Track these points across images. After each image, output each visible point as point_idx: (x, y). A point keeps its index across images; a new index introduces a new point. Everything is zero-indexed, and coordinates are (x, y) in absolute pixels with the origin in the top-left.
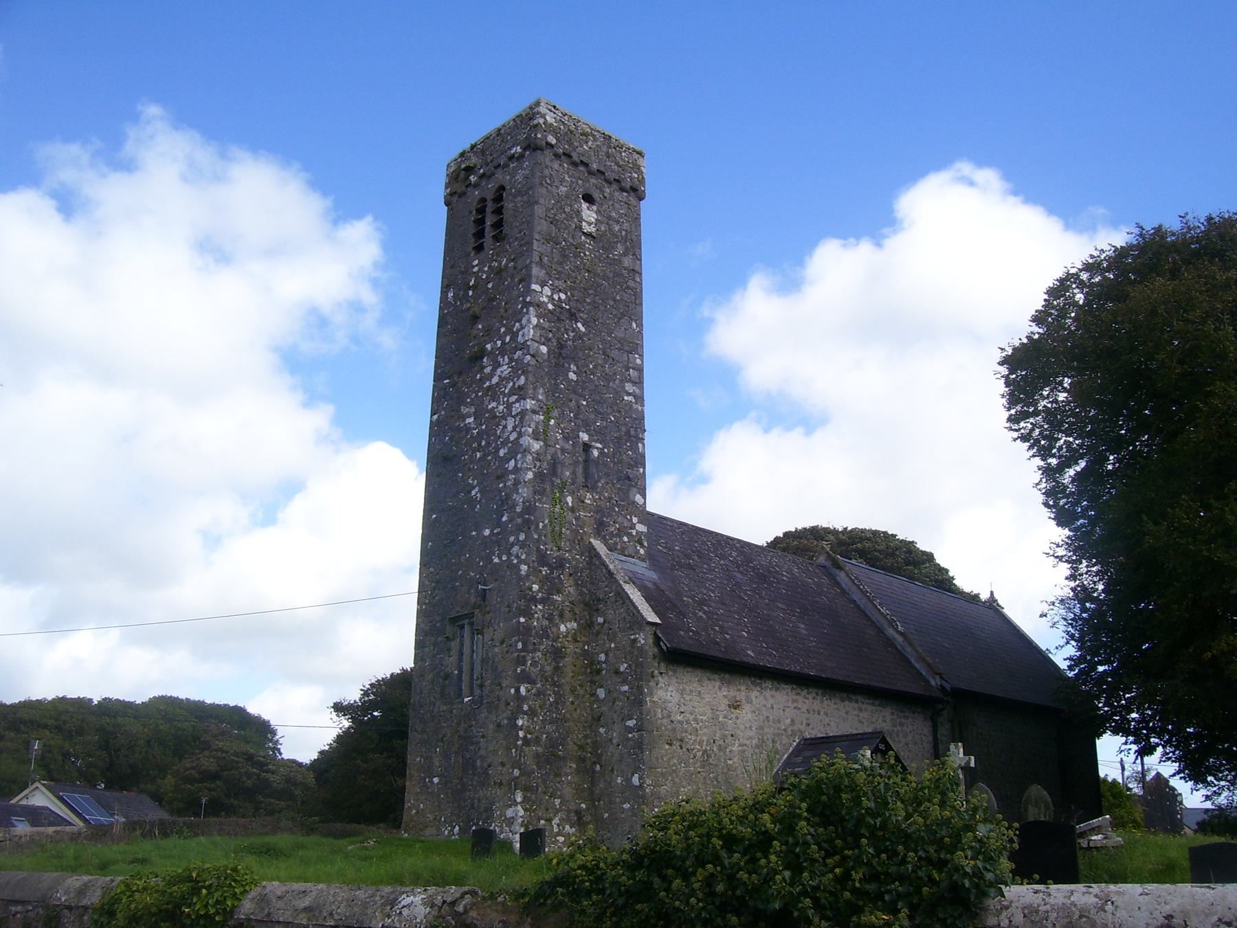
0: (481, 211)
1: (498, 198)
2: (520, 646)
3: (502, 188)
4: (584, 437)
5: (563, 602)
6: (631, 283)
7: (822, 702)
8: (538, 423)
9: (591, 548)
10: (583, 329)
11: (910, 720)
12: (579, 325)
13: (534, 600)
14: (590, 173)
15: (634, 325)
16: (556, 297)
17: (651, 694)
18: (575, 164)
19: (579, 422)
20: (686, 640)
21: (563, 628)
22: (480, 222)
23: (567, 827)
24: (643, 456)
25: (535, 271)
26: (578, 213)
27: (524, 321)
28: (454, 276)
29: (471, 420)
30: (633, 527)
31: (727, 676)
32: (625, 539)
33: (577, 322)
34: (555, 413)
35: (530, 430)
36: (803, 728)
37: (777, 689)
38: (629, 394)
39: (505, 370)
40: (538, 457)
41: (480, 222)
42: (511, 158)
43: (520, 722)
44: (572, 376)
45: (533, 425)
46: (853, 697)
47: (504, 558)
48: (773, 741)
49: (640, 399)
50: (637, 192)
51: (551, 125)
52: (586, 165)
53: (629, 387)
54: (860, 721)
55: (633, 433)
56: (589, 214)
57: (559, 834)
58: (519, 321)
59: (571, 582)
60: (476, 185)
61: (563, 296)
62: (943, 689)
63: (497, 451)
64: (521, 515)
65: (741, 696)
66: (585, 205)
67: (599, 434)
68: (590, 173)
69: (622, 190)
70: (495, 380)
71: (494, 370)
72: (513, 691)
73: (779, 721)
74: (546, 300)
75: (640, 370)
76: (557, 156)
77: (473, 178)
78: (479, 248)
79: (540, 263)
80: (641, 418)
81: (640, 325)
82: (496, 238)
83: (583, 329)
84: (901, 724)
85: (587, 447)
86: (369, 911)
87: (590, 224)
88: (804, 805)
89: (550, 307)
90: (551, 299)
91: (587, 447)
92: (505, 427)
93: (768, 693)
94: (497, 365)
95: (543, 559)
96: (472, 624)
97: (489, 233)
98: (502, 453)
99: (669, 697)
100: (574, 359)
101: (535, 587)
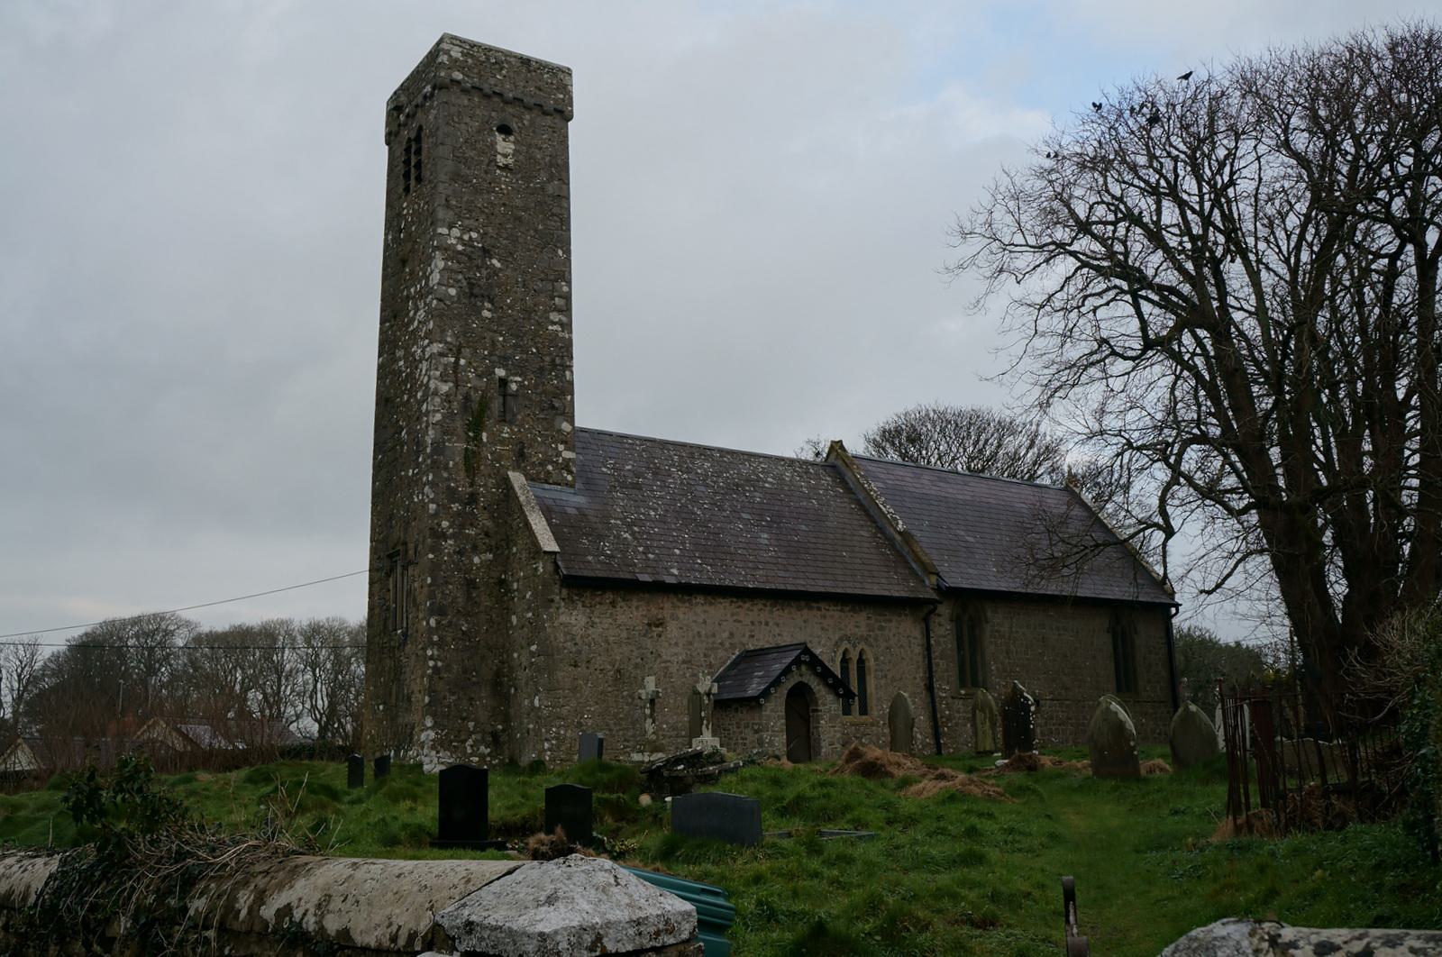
1: (418, 139)
2: (429, 580)
4: (500, 372)
5: (477, 534)
6: (556, 210)
7: (771, 612)
8: (446, 365)
9: (507, 481)
10: (498, 265)
11: (894, 624)
12: (495, 261)
13: (444, 536)
14: (506, 102)
15: (560, 252)
16: (466, 237)
17: (551, 618)
18: (487, 96)
19: (495, 358)
20: (592, 566)
21: (476, 560)
23: (482, 748)
24: (571, 383)
25: (441, 213)
26: (493, 144)
27: (433, 266)
29: (401, 363)
30: (559, 454)
31: (647, 595)
32: (550, 468)
33: (491, 258)
34: (466, 351)
35: (438, 373)
36: (745, 640)
37: (711, 604)
38: (555, 323)
39: (421, 314)
40: (447, 398)
43: (429, 653)
44: (486, 314)
45: (441, 368)
46: (814, 605)
48: (705, 655)
49: (567, 326)
51: (457, 60)
52: (500, 95)
53: (554, 316)
54: (822, 629)
55: (558, 361)
57: (472, 755)
58: (430, 265)
59: (486, 515)
60: (405, 125)
61: (474, 235)
64: (431, 455)
66: (499, 137)
67: (520, 369)
68: (506, 102)
69: (546, 113)
70: (416, 323)
71: (415, 314)
72: (425, 623)
73: (714, 635)
74: (454, 241)
76: (465, 91)
79: (448, 206)
80: (568, 345)
81: (568, 252)
83: (498, 265)
84: (881, 628)
85: (503, 382)
87: (505, 156)
89: (460, 248)
90: (460, 239)
91: (503, 382)
93: (699, 609)
95: (452, 495)
99: (573, 622)
101: (445, 524)
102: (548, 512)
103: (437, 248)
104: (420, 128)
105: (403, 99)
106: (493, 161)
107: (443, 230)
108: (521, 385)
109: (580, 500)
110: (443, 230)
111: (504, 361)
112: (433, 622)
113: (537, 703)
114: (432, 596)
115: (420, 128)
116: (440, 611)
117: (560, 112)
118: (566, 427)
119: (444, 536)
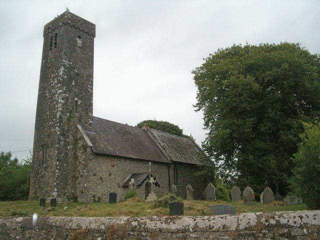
4: (76, 99)
9: (77, 127)
18: (76, 28)
21: (69, 147)
26: (76, 41)
39: (56, 82)
44: (73, 84)
49: (92, 89)
53: (89, 86)
61: (71, 63)
66: (78, 39)
67: (80, 99)
70: (54, 84)
91: (77, 101)
102: (88, 135)
103: (62, 65)
104: (57, 34)
105: (51, 26)
106: (76, 44)
107: (64, 61)
108: (81, 103)
109: (94, 133)
110: (64, 61)
111: (77, 96)
112: (58, 163)
113: (85, 185)
114: (58, 156)
115: (57, 34)
116: (59, 160)
117: (92, 35)
118: (91, 114)
119: (61, 141)
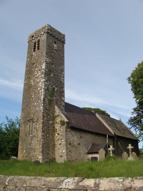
0: (35, 44)
1: (39, 42)
3: (39, 40)
4: (54, 87)
6: (62, 59)
22: (35, 46)
28: (30, 56)
38: (62, 79)
41: (35, 46)
42: (41, 34)
44: (52, 75)
47: (39, 109)
49: (64, 80)
50: (63, 42)
56: (55, 46)
62: (115, 135)
63: (38, 88)
65: (82, 136)
66: (54, 44)
71: (37, 73)
75: (64, 75)
77: (33, 38)
78: (34, 51)
82: (38, 49)
86: (61, 91)
88: (110, 149)
89: (48, 62)
91: (54, 88)
92: (39, 84)
94: (38, 73)
96: (32, 121)
97: (37, 48)
98: (39, 89)
100: (52, 72)
